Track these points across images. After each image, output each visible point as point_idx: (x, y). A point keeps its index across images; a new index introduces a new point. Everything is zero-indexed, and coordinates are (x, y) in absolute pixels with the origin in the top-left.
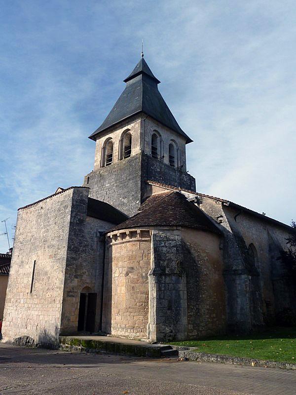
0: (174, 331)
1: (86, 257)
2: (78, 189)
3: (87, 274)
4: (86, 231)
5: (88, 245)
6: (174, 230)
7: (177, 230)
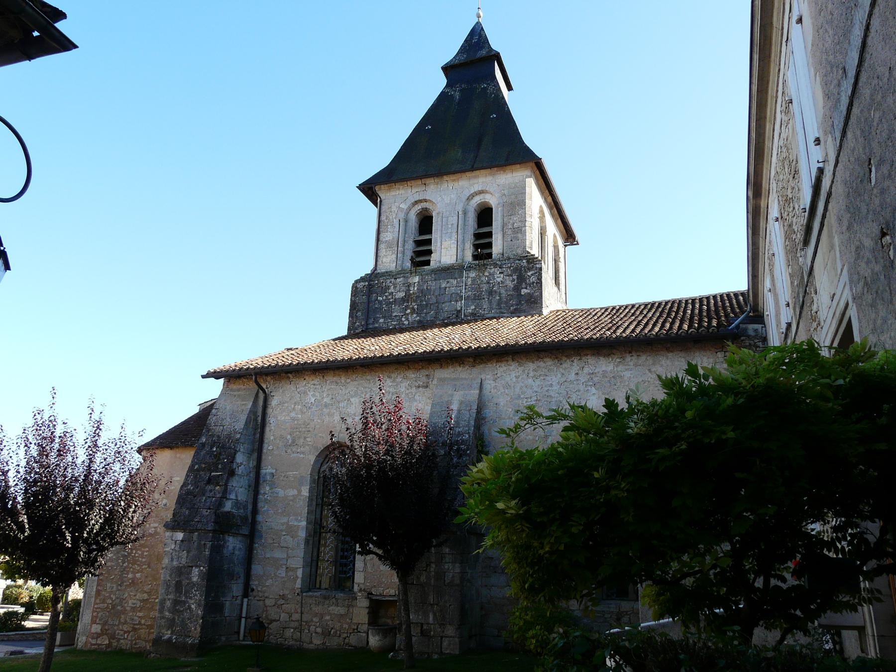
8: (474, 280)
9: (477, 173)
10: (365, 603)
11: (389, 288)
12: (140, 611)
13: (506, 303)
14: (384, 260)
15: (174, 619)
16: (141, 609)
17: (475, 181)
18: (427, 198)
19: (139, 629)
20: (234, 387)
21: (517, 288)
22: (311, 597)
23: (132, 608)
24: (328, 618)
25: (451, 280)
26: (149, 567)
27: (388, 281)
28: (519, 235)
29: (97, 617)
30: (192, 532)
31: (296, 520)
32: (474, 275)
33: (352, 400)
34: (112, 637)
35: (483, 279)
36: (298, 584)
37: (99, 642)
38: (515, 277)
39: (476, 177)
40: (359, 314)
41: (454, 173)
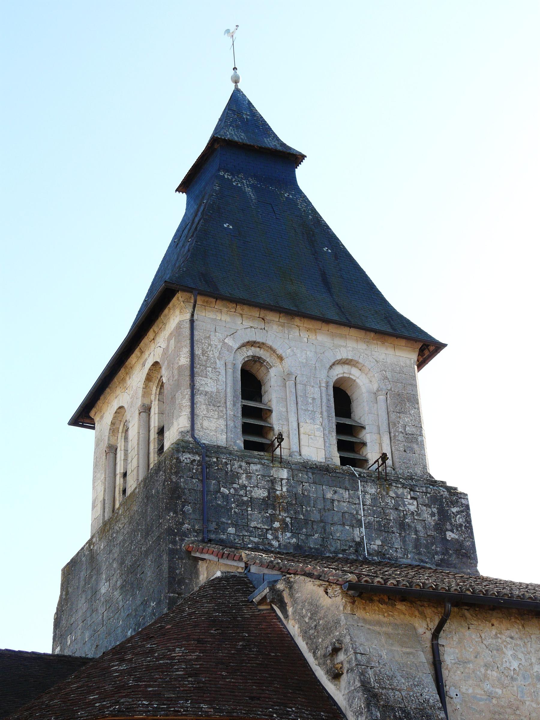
8: (374, 499)
9: (345, 331)
11: (237, 476)
13: (427, 547)
14: (206, 424)
17: (341, 342)
18: (270, 343)
20: (360, 613)
21: (440, 528)
25: (341, 491)
27: (236, 465)
28: (415, 446)
32: (373, 491)
35: (388, 500)
38: (435, 510)
39: (315, 331)
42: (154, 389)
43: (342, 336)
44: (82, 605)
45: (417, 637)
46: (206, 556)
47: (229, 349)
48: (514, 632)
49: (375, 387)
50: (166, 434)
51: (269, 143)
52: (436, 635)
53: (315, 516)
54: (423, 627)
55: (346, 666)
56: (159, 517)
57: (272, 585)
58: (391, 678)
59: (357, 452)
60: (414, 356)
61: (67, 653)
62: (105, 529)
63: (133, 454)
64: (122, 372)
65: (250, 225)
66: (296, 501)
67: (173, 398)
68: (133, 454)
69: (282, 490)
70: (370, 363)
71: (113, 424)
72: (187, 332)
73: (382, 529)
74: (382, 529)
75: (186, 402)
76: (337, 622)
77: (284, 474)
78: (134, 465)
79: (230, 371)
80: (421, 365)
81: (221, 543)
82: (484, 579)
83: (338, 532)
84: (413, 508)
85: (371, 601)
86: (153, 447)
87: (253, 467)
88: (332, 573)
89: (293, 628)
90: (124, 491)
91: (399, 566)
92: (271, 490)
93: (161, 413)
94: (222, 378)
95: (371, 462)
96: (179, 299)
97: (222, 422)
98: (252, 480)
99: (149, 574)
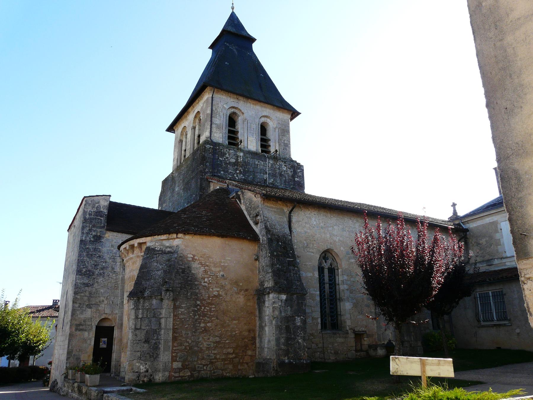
0: (150, 371)
1: (105, 282)
2: (93, 198)
3: (106, 302)
4: (104, 250)
5: (107, 267)
6: (175, 239)
7: (177, 238)
8: (272, 165)
9: (266, 105)
10: (353, 336)
11: (226, 154)
12: (214, 350)
13: (288, 182)
14: (215, 135)
15: (288, 349)
16: (215, 348)
18: (239, 108)
19: (216, 362)
20: (266, 204)
21: (293, 176)
22: (326, 334)
23: (207, 348)
24: (336, 344)
26: (217, 319)
29: (176, 356)
30: (293, 294)
31: (314, 290)
32: (272, 162)
33: (335, 227)
34: (193, 369)
36: (319, 327)
37: (181, 374)
39: (256, 104)
40: (208, 164)
41: (274, 105)
42: (197, 121)
43: (265, 107)
44: (169, 194)
45: (284, 213)
46: (213, 181)
47: (225, 108)
48: (315, 213)
49: (275, 126)
50: (201, 137)
51: (245, 34)
52: (290, 212)
53: (251, 170)
54: (286, 210)
55: (260, 221)
56: (197, 166)
57: (237, 192)
58: (275, 225)
59: (267, 148)
60: (289, 116)
61: (163, 209)
62: (178, 168)
63: (189, 143)
64: (186, 114)
65: (234, 64)
66: (245, 164)
67: (204, 125)
68: (189, 143)
69: (241, 160)
70: (274, 118)
71: (182, 132)
72: (211, 101)
73: (273, 175)
74: (273, 175)
75: (209, 127)
76: (258, 206)
77: (242, 154)
78: (189, 147)
79: (225, 117)
80: (291, 119)
81: (219, 177)
82: (307, 195)
83: (259, 176)
84: (285, 169)
85: (270, 200)
86: (196, 141)
87: (231, 151)
88: (257, 189)
89: (243, 207)
90: (185, 156)
91: (279, 189)
92: (237, 160)
93: (199, 130)
94: (222, 119)
95: (272, 152)
96: (208, 89)
97: (221, 135)
98: (230, 156)
99: (193, 185)
